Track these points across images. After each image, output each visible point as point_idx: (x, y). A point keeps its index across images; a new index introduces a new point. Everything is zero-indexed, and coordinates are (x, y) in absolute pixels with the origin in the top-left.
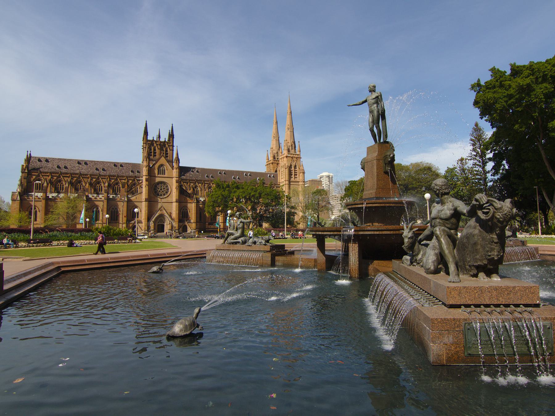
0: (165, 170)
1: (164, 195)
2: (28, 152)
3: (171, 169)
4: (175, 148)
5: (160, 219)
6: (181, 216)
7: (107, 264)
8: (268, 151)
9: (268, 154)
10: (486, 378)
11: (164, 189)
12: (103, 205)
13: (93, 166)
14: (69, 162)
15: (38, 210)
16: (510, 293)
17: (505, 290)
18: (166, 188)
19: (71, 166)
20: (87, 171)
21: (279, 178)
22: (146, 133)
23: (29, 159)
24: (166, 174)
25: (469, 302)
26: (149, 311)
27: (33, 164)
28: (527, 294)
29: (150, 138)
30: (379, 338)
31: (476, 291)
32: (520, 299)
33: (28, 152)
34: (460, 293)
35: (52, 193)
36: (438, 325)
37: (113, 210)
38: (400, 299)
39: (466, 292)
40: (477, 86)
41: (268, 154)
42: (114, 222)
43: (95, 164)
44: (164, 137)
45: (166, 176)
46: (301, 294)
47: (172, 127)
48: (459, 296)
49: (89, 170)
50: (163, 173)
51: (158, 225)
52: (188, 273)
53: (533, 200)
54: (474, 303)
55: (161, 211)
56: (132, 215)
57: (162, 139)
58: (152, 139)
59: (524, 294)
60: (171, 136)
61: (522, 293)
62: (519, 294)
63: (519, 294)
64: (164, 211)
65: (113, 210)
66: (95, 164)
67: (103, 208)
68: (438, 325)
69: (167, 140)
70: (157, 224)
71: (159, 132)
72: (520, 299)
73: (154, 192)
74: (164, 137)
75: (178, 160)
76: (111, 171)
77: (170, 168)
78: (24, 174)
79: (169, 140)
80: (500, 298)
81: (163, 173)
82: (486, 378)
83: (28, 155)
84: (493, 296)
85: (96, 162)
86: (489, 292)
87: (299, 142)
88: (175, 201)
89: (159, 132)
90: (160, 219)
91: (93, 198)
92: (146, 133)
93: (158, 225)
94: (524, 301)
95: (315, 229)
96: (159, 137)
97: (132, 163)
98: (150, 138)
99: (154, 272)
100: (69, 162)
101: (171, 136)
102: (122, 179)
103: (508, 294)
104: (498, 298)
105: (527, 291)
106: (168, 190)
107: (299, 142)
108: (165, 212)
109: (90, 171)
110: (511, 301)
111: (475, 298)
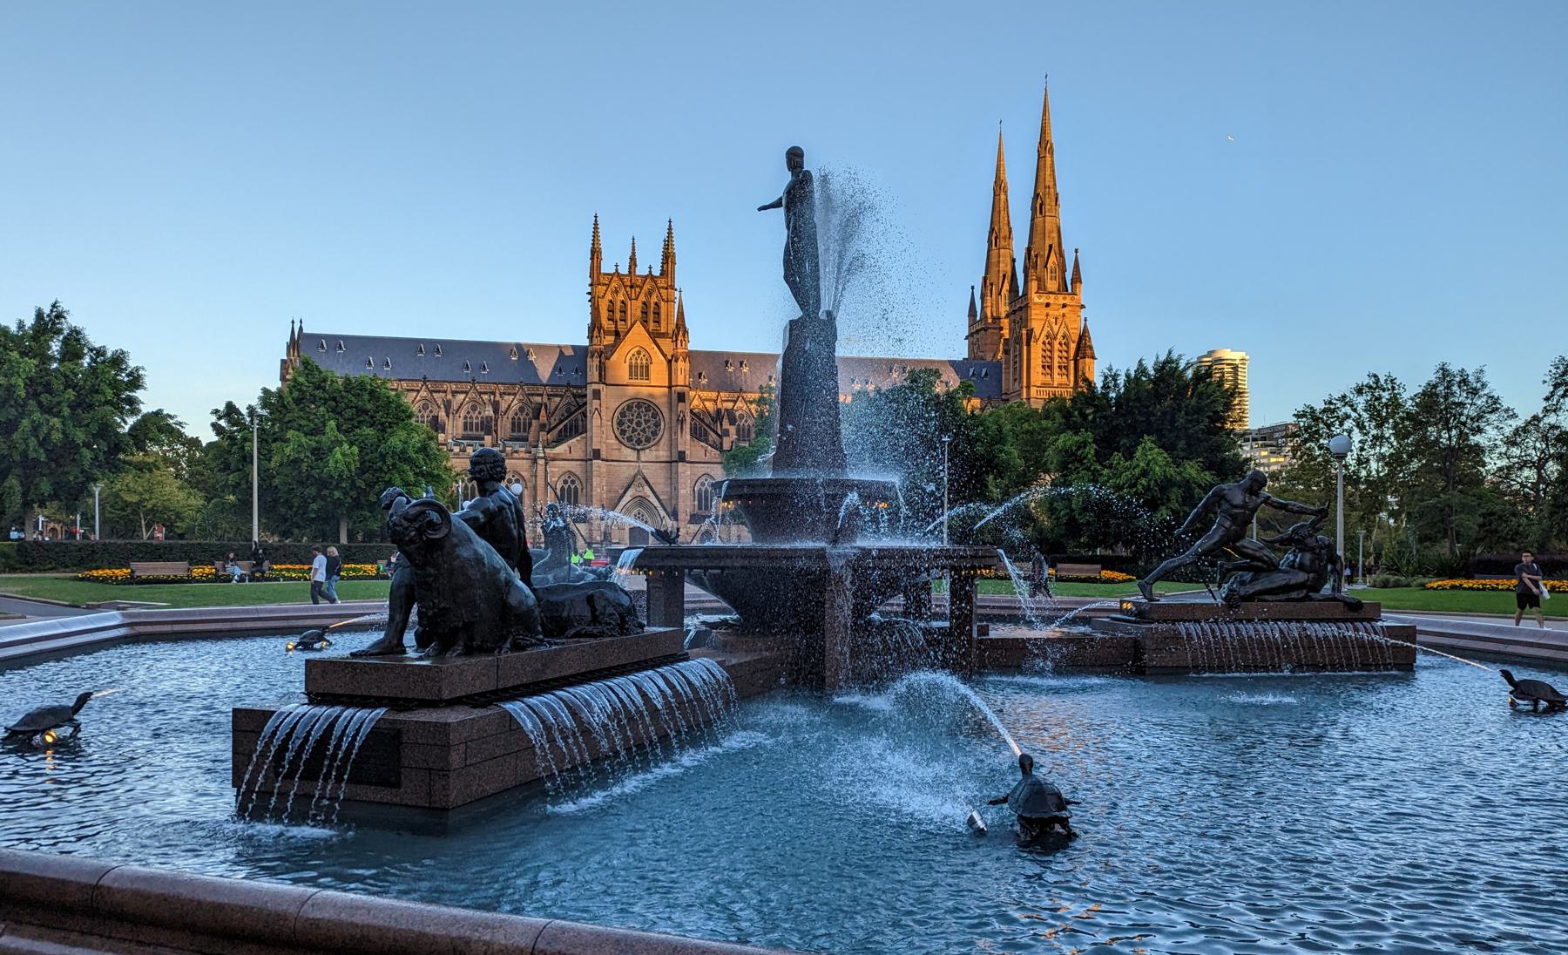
2: (293, 322)
6: (696, 503)
7: (1526, 648)
11: (647, 422)
18: (653, 421)
21: (1007, 379)
22: (595, 253)
23: (298, 342)
24: (652, 376)
29: (607, 267)
30: (424, 935)
33: (293, 322)
53: (790, 427)
57: (641, 270)
60: (668, 257)
64: (647, 488)
65: (703, 489)
73: (617, 433)
74: (650, 262)
75: (681, 329)
87: (1076, 251)
92: (595, 253)
98: (607, 267)
101: (668, 257)
107: (1076, 251)
108: (649, 492)
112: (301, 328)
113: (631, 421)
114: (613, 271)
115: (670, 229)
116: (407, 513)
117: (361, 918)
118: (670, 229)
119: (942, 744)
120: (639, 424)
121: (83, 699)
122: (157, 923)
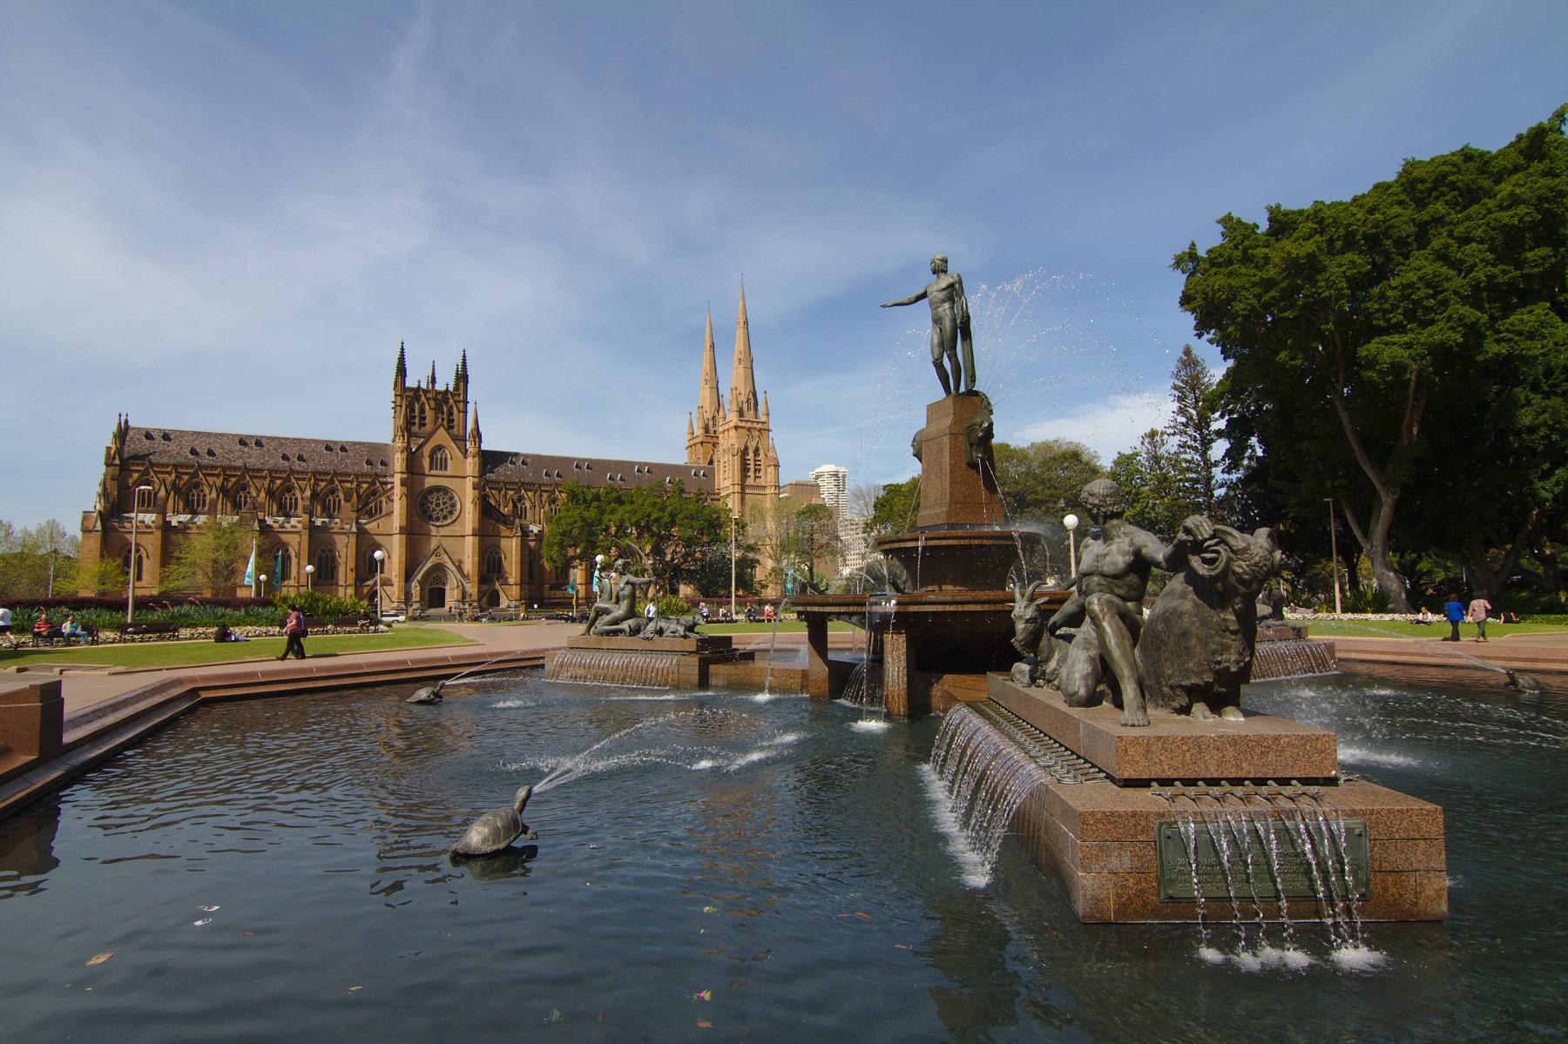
0: (446, 459)
2: (120, 415)
4: (470, 408)
5: (435, 575)
10: (1210, 954)
11: (444, 503)
12: (300, 543)
18: (449, 503)
22: (402, 371)
23: (123, 433)
25: (1170, 774)
31: (1185, 748)
33: (120, 415)
34: (1148, 752)
40: (1188, 260)
46: (769, 755)
47: (464, 356)
52: (501, 705)
57: (440, 387)
60: (462, 377)
62: (1288, 754)
63: (1288, 754)
66: (281, 444)
74: (446, 381)
77: (459, 454)
78: (111, 469)
80: (1244, 765)
82: (1210, 954)
83: (120, 424)
86: (1218, 750)
87: (765, 392)
88: (398, 531)
90: (435, 575)
91: (276, 525)
92: (402, 371)
95: (803, 599)
99: (421, 702)
101: (462, 377)
107: (765, 392)
109: (267, 462)
111: (1183, 764)
112: (126, 422)
114: (416, 386)
115: (402, 349)
116: (1039, 544)
117: (131, 729)
118: (402, 349)
119: (1218, 647)
120: (438, 505)
121: (1445, 640)
122: (108, 732)
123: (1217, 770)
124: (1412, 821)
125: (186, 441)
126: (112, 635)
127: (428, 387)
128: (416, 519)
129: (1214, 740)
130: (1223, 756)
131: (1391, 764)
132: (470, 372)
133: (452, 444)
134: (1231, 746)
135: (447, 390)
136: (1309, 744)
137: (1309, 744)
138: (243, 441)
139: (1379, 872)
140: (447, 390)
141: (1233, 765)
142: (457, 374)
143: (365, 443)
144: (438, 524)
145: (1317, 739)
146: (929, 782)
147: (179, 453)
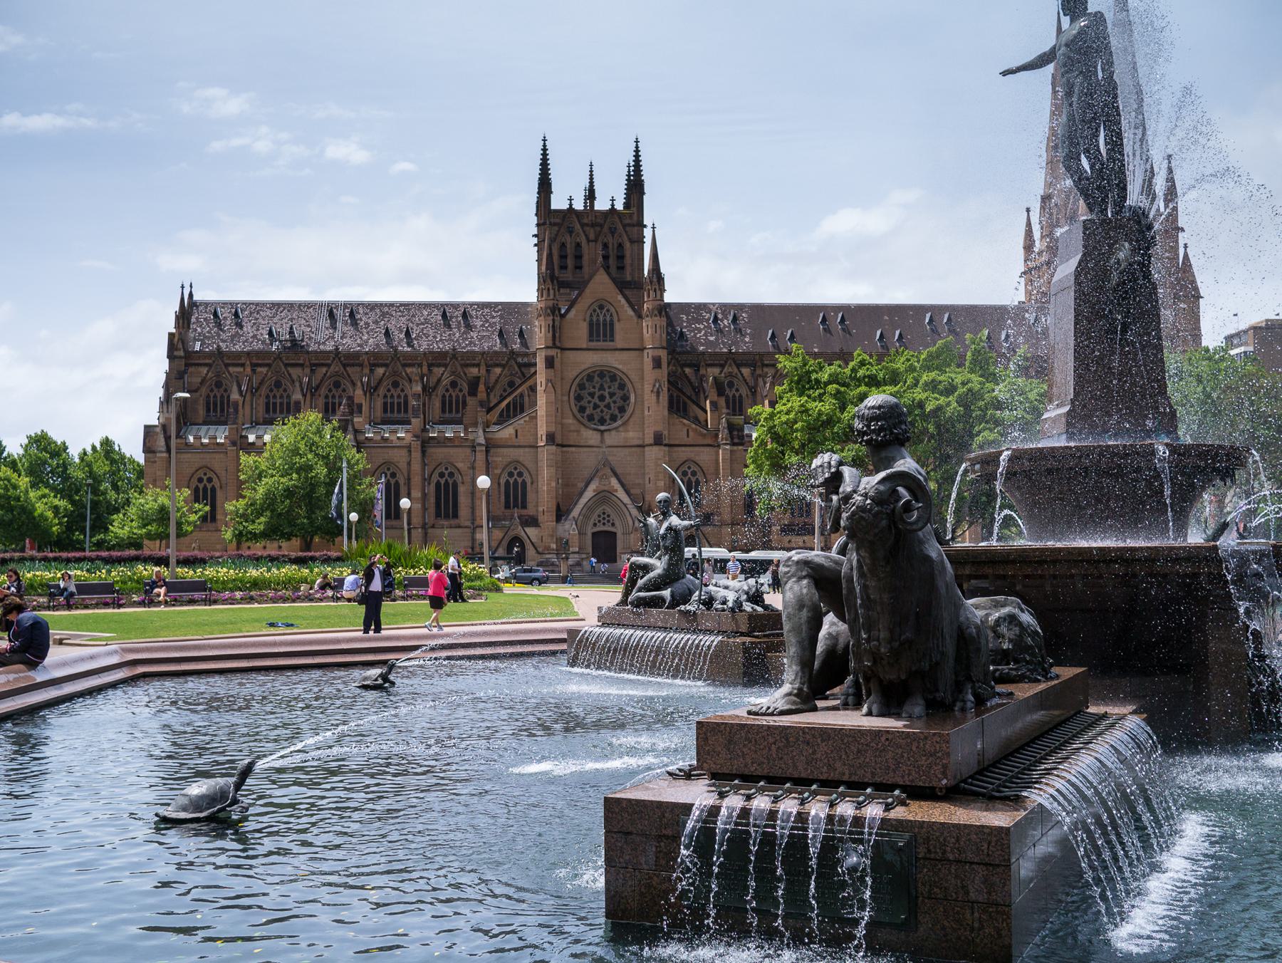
0: (612, 321)
1: (614, 418)
2: (183, 287)
3: (635, 319)
4: (647, 233)
5: (599, 511)
8: (1028, 210)
9: (1029, 224)
11: (612, 395)
12: (409, 464)
13: (376, 322)
14: (304, 315)
15: (217, 486)
16: (866, 751)
17: (850, 739)
18: (619, 393)
19: (309, 326)
20: (359, 341)
23: (186, 312)
24: (618, 336)
25: (753, 769)
26: (295, 809)
27: (199, 329)
28: (913, 757)
29: (558, 202)
31: (771, 740)
32: (894, 771)
33: (183, 287)
34: (730, 742)
35: (257, 424)
36: (620, 818)
37: (442, 482)
38: (432, 726)
39: (746, 739)
41: (1029, 224)
42: (446, 523)
43: (384, 315)
44: (611, 195)
45: (619, 343)
47: (637, 151)
48: (729, 750)
49: (365, 338)
50: (605, 335)
51: (594, 534)
54: (765, 772)
55: (601, 478)
56: (503, 497)
57: (601, 204)
58: (565, 206)
59: (905, 755)
60: (635, 186)
61: (900, 751)
62: (890, 755)
63: (890, 755)
64: (614, 482)
65: (442, 482)
66: (384, 315)
67: (409, 475)
68: (620, 818)
69: (619, 206)
70: (590, 530)
71: (591, 175)
72: (894, 771)
74: (611, 195)
76: (435, 337)
77: (631, 312)
78: (177, 361)
79: (627, 205)
80: (838, 765)
81: (605, 335)
83: (182, 299)
84: (819, 756)
85: (386, 309)
86: (808, 744)
88: (652, 441)
89: (591, 175)
90: (599, 511)
93: (594, 534)
94: (903, 777)
96: (591, 195)
97: (501, 304)
98: (558, 202)
100: (304, 315)
101: (635, 186)
102: (467, 365)
103: (859, 751)
104: (831, 762)
105: (914, 749)
106: (626, 398)
109: (367, 342)
110: (869, 775)
111: (768, 759)
112: (191, 295)
113: (612, 395)
115: (545, 149)
118: (545, 149)
120: (602, 398)
123: (806, 769)
124: (969, 840)
125: (264, 318)
126: (43, 600)
127: (585, 206)
128: (570, 421)
129: (804, 733)
130: (814, 752)
131: (1048, 772)
132: (646, 176)
133: (620, 297)
134: (823, 741)
135: (613, 208)
136: (915, 744)
137: (915, 744)
138: (331, 311)
139: (929, 898)
140: (613, 208)
141: (825, 764)
142: (628, 180)
143: (497, 304)
144: (602, 428)
145: (926, 738)
146: (1194, 861)
147: (254, 336)
